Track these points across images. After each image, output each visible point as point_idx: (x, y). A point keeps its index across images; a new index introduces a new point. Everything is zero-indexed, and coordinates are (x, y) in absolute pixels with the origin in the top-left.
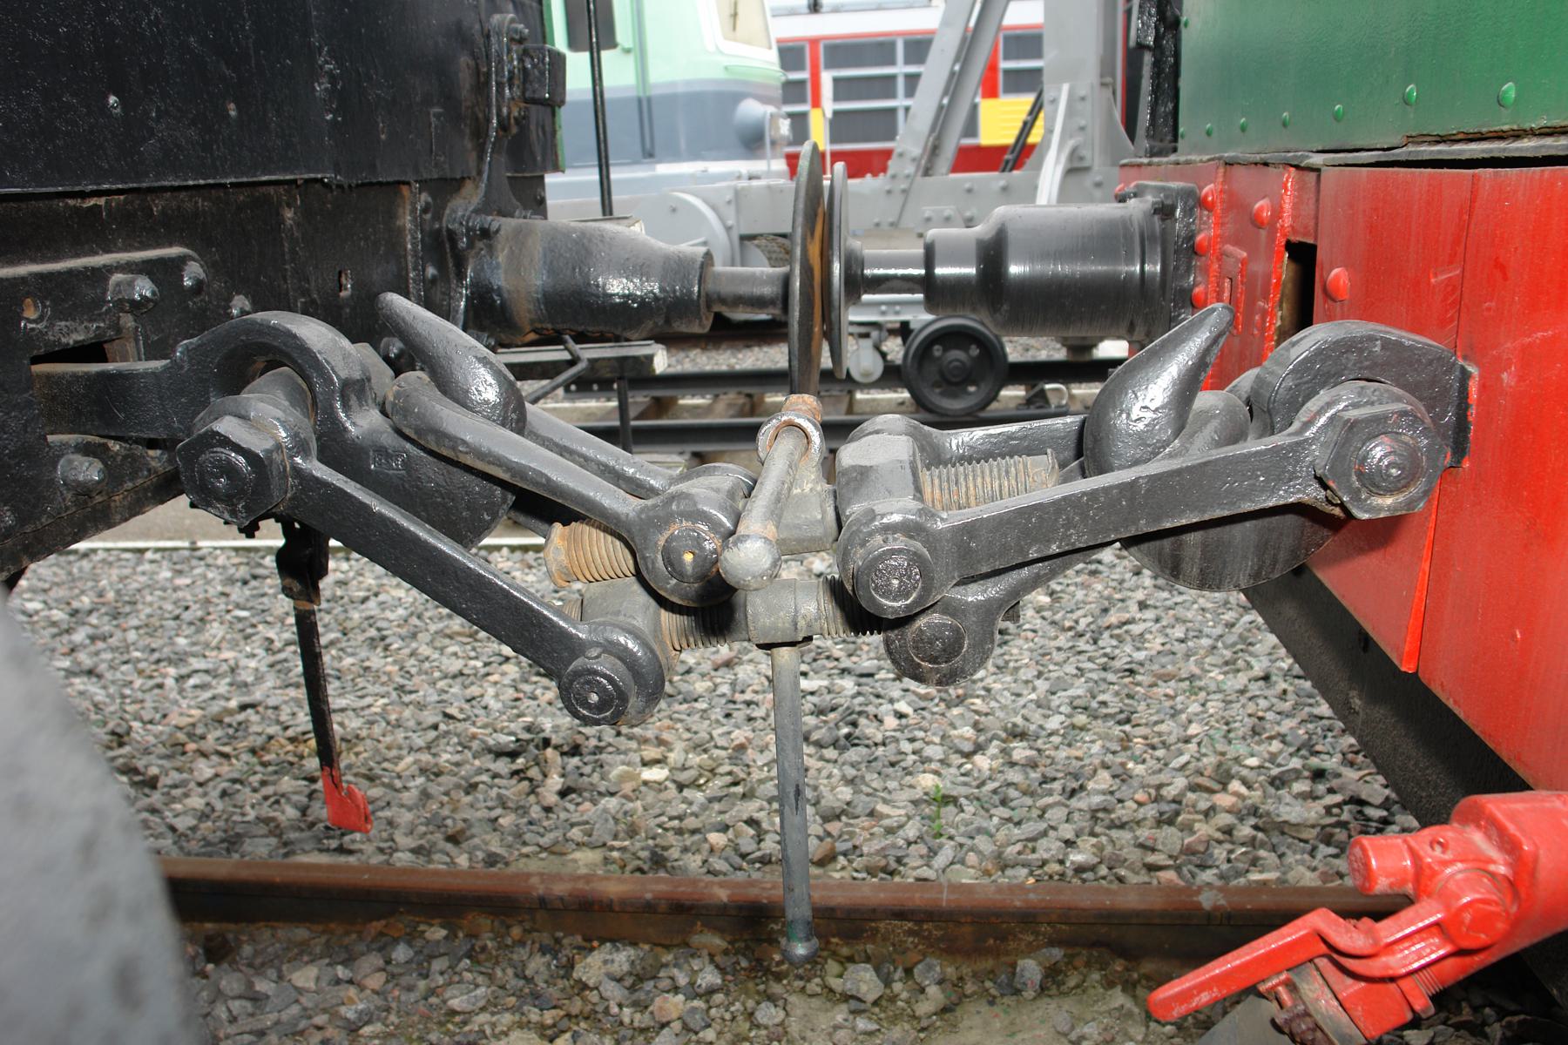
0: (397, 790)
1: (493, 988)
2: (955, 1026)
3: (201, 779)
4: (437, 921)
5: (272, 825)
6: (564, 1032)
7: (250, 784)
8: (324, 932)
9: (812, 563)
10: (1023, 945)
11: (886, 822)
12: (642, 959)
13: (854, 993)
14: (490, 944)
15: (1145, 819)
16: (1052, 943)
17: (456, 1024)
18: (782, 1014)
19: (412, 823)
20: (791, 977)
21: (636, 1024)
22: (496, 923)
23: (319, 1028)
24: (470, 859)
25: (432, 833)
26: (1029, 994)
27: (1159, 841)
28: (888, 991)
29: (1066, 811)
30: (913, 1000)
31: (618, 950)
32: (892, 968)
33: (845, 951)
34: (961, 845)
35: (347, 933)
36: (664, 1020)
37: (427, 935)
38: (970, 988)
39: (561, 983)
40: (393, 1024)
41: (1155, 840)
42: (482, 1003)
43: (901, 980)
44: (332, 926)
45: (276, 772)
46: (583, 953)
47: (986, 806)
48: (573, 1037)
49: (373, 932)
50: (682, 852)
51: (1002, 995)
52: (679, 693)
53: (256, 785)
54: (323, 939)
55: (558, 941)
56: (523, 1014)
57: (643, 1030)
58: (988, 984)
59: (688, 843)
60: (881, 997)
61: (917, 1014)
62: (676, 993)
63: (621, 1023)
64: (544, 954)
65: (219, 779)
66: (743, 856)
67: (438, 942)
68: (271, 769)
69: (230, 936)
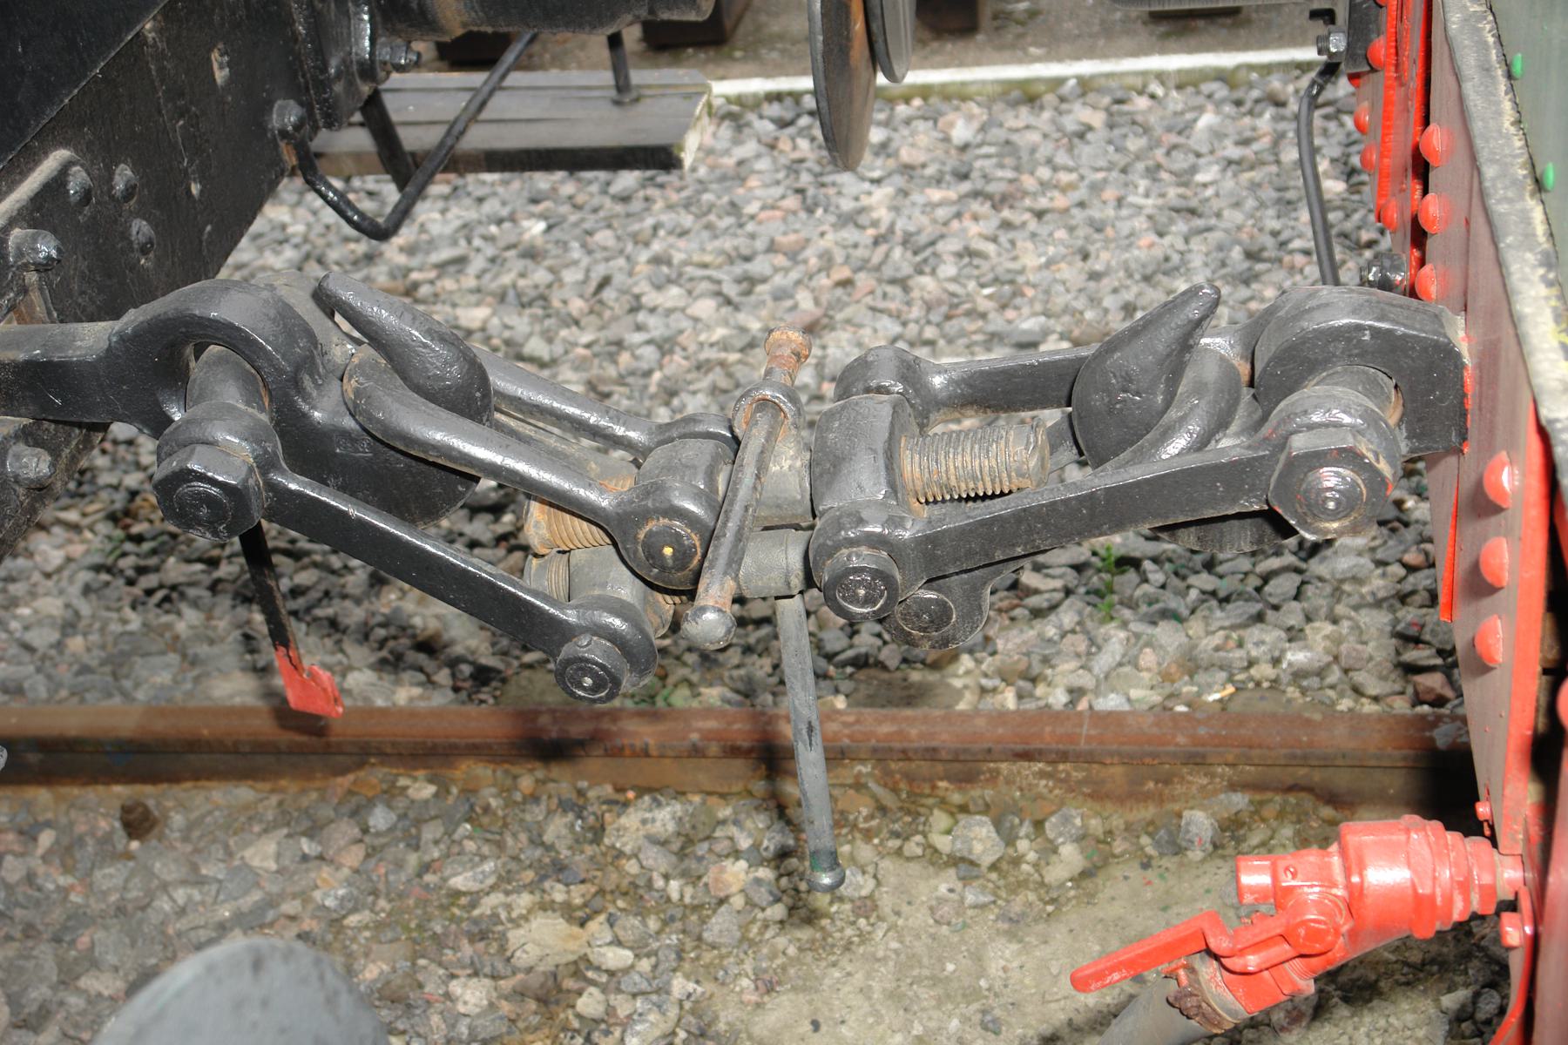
0: (333, 572)
1: (504, 859)
2: (1092, 896)
3: (49, 569)
4: (421, 773)
5: (168, 635)
6: (597, 912)
7: (121, 571)
8: (273, 791)
9: (952, 125)
10: (1194, 789)
11: (1033, 601)
12: (692, 815)
13: (965, 854)
14: (494, 802)
15: (1413, 593)
16: (1233, 787)
17: (463, 908)
18: (871, 883)
19: (366, 624)
20: (884, 834)
21: (687, 900)
22: (499, 773)
23: (293, 918)
24: (453, 675)
25: (395, 638)
26: (1196, 855)
27: (1427, 629)
28: (1011, 851)
29: (1297, 579)
30: (1043, 863)
31: (659, 805)
32: (1017, 821)
33: (956, 798)
34: (1137, 636)
35: (303, 791)
36: (722, 895)
37: (410, 792)
38: (1119, 846)
39: (590, 850)
40: (383, 910)
41: (1423, 626)
42: (491, 881)
43: (1027, 836)
44: (283, 783)
45: (154, 552)
46: (616, 808)
47: (1183, 571)
48: (608, 920)
49: (339, 791)
50: (744, 653)
51: (1162, 855)
52: (737, 385)
53: (130, 573)
54: (274, 799)
55: (581, 793)
56: (544, 891)
57: (696, 908)
58: (1145, 840)
59: (752, 640)
60: (999, 860)
61: (1046, 880)
62: (737, 859)
63: (669, 900)
64: (565, 811)
65: (73, 566)
66: (830, 657)
67: (426, 802)
68: (146, 546)
69: (151, 803)
